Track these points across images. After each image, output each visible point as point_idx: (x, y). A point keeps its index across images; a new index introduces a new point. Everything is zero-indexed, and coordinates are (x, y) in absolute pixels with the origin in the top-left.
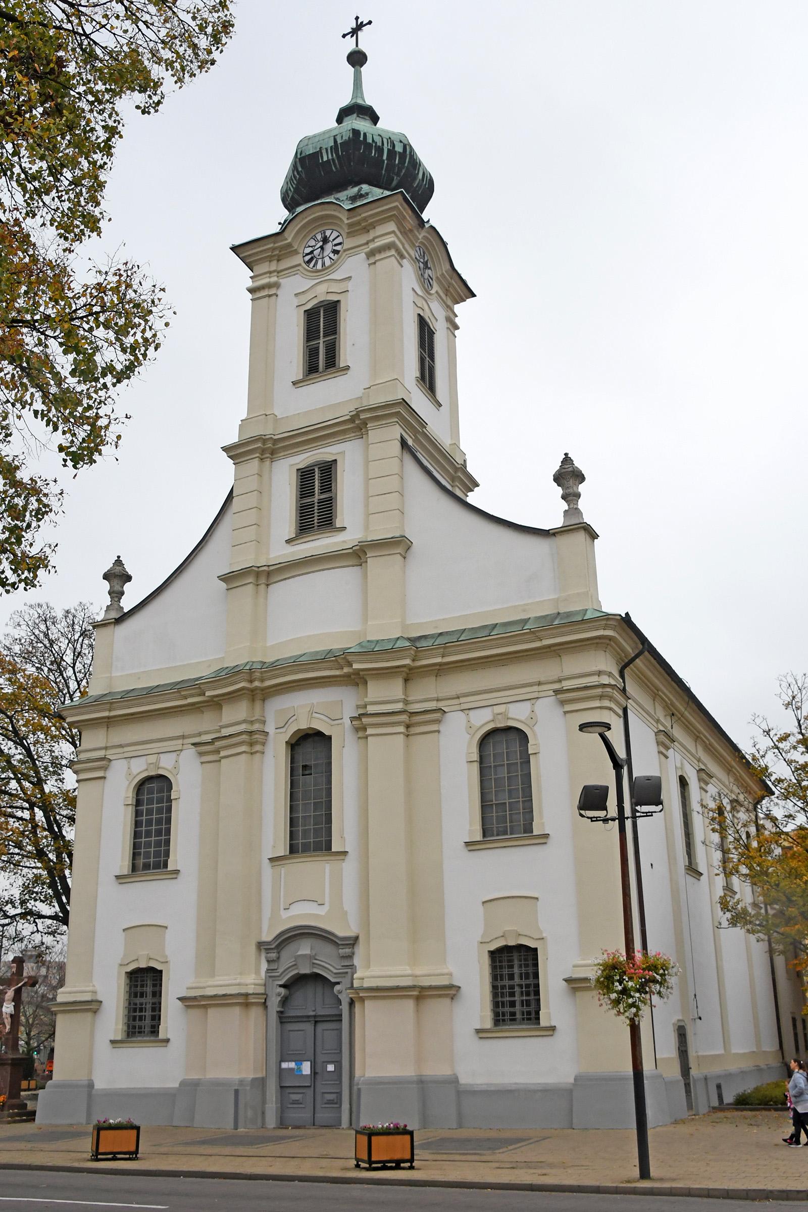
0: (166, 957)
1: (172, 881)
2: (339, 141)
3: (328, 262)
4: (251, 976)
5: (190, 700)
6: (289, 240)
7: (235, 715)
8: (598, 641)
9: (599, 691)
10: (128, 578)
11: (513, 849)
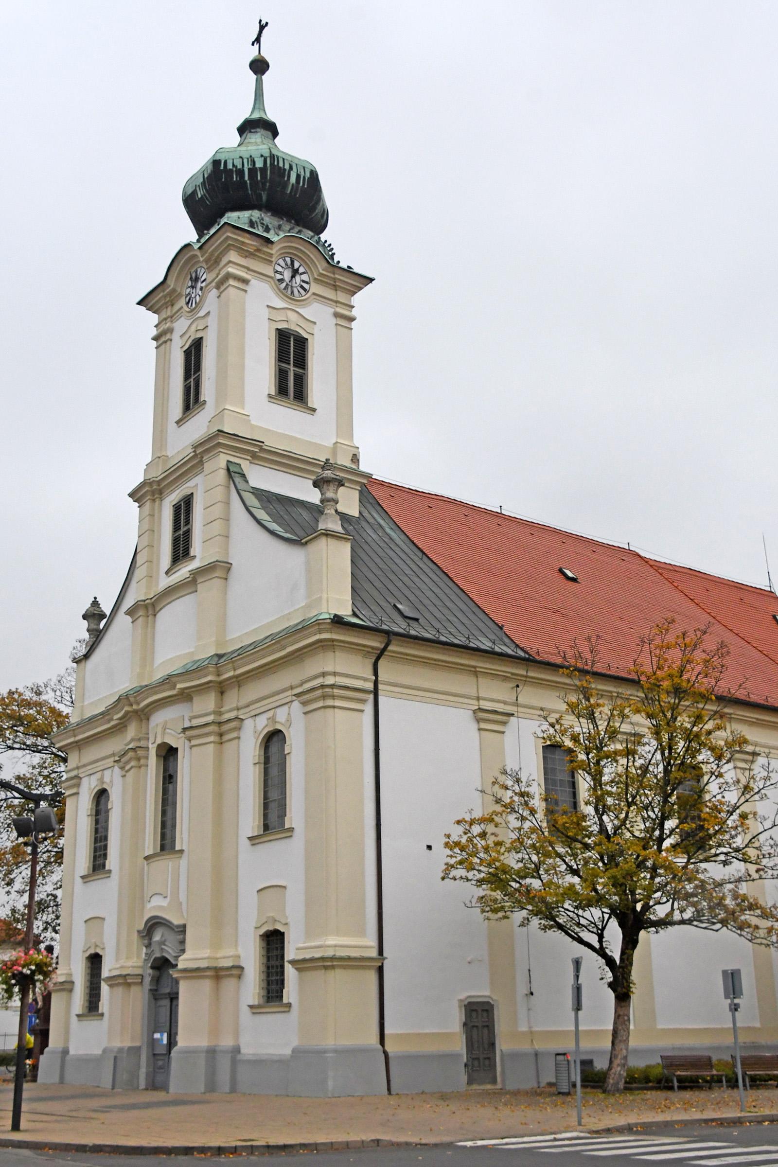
0: (103, 944)
6: (273, 252)
9: (319, 692)
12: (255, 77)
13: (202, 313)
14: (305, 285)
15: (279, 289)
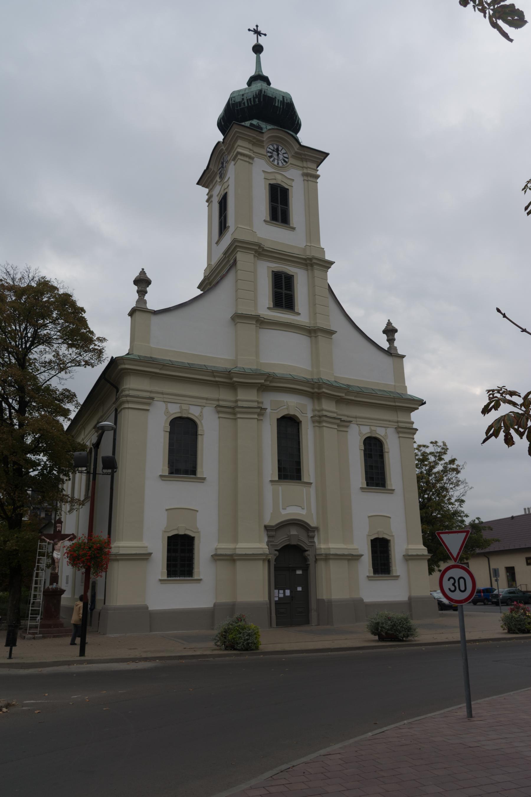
0: (198, 529)
1: (390, 495)
2: (285, 101)
3: (280, 164)
4: (260, 545)
5: (217, 379)
6: (264, 139)
7: (247, 397)
8: (154, 374)
10: (396, 331)
11: (174, 482)
12: (255, 55)
13: (226, 180)
14: (286, 160)
15: (270, 161)
